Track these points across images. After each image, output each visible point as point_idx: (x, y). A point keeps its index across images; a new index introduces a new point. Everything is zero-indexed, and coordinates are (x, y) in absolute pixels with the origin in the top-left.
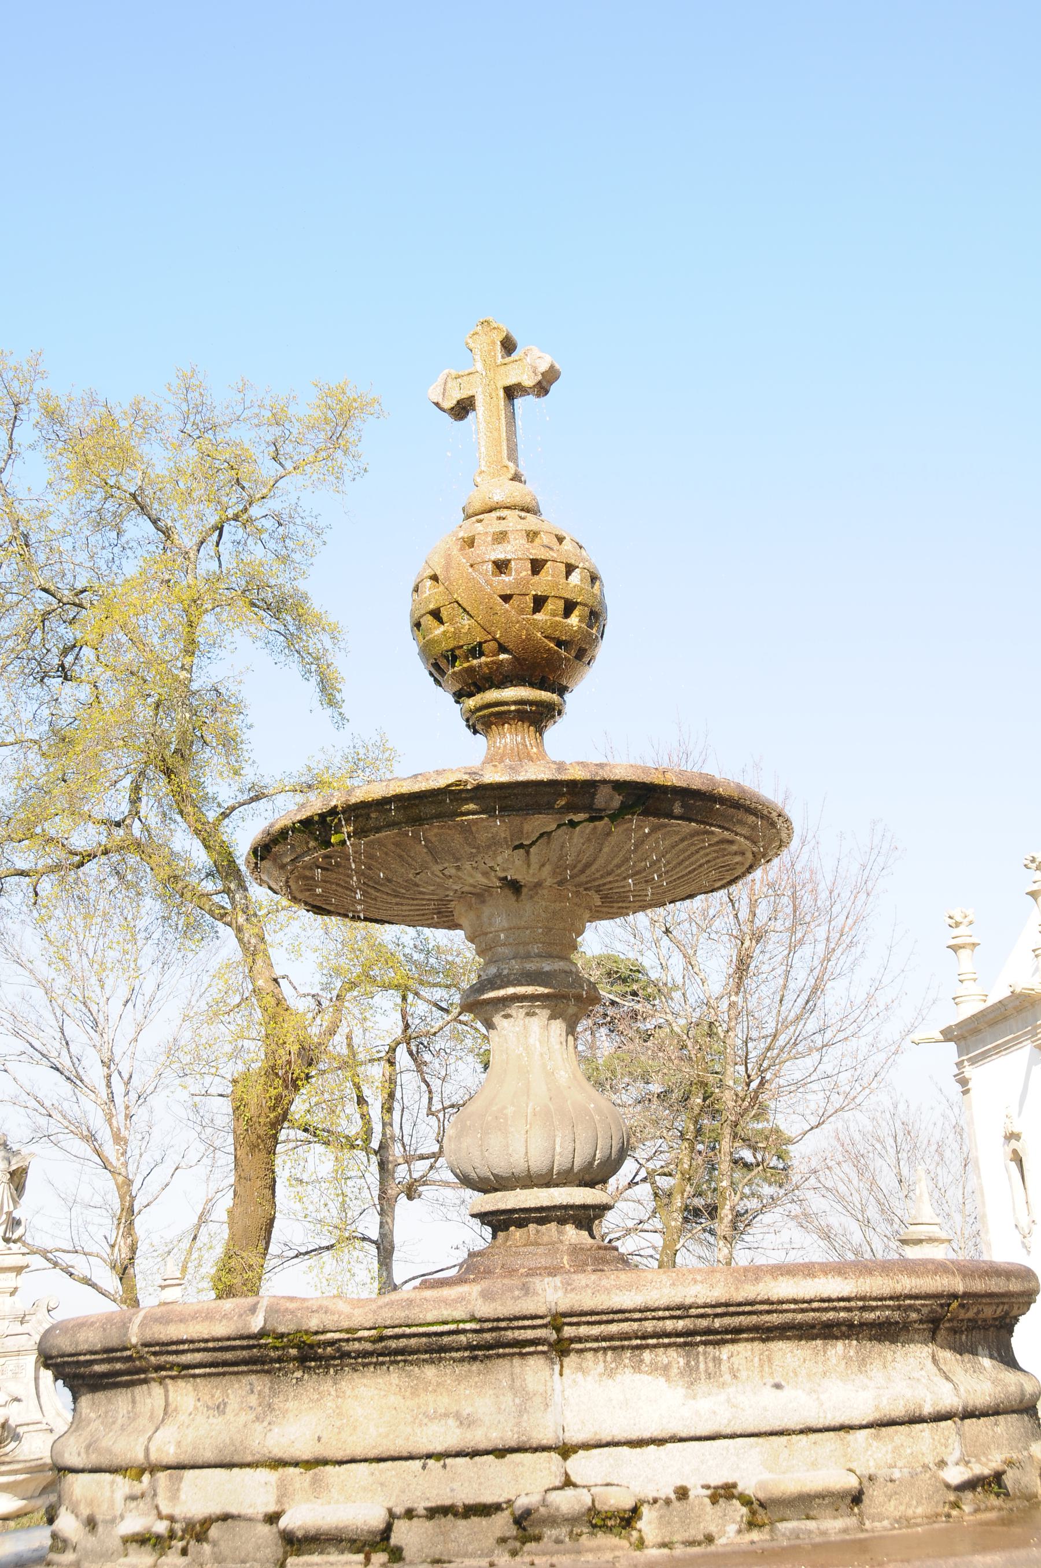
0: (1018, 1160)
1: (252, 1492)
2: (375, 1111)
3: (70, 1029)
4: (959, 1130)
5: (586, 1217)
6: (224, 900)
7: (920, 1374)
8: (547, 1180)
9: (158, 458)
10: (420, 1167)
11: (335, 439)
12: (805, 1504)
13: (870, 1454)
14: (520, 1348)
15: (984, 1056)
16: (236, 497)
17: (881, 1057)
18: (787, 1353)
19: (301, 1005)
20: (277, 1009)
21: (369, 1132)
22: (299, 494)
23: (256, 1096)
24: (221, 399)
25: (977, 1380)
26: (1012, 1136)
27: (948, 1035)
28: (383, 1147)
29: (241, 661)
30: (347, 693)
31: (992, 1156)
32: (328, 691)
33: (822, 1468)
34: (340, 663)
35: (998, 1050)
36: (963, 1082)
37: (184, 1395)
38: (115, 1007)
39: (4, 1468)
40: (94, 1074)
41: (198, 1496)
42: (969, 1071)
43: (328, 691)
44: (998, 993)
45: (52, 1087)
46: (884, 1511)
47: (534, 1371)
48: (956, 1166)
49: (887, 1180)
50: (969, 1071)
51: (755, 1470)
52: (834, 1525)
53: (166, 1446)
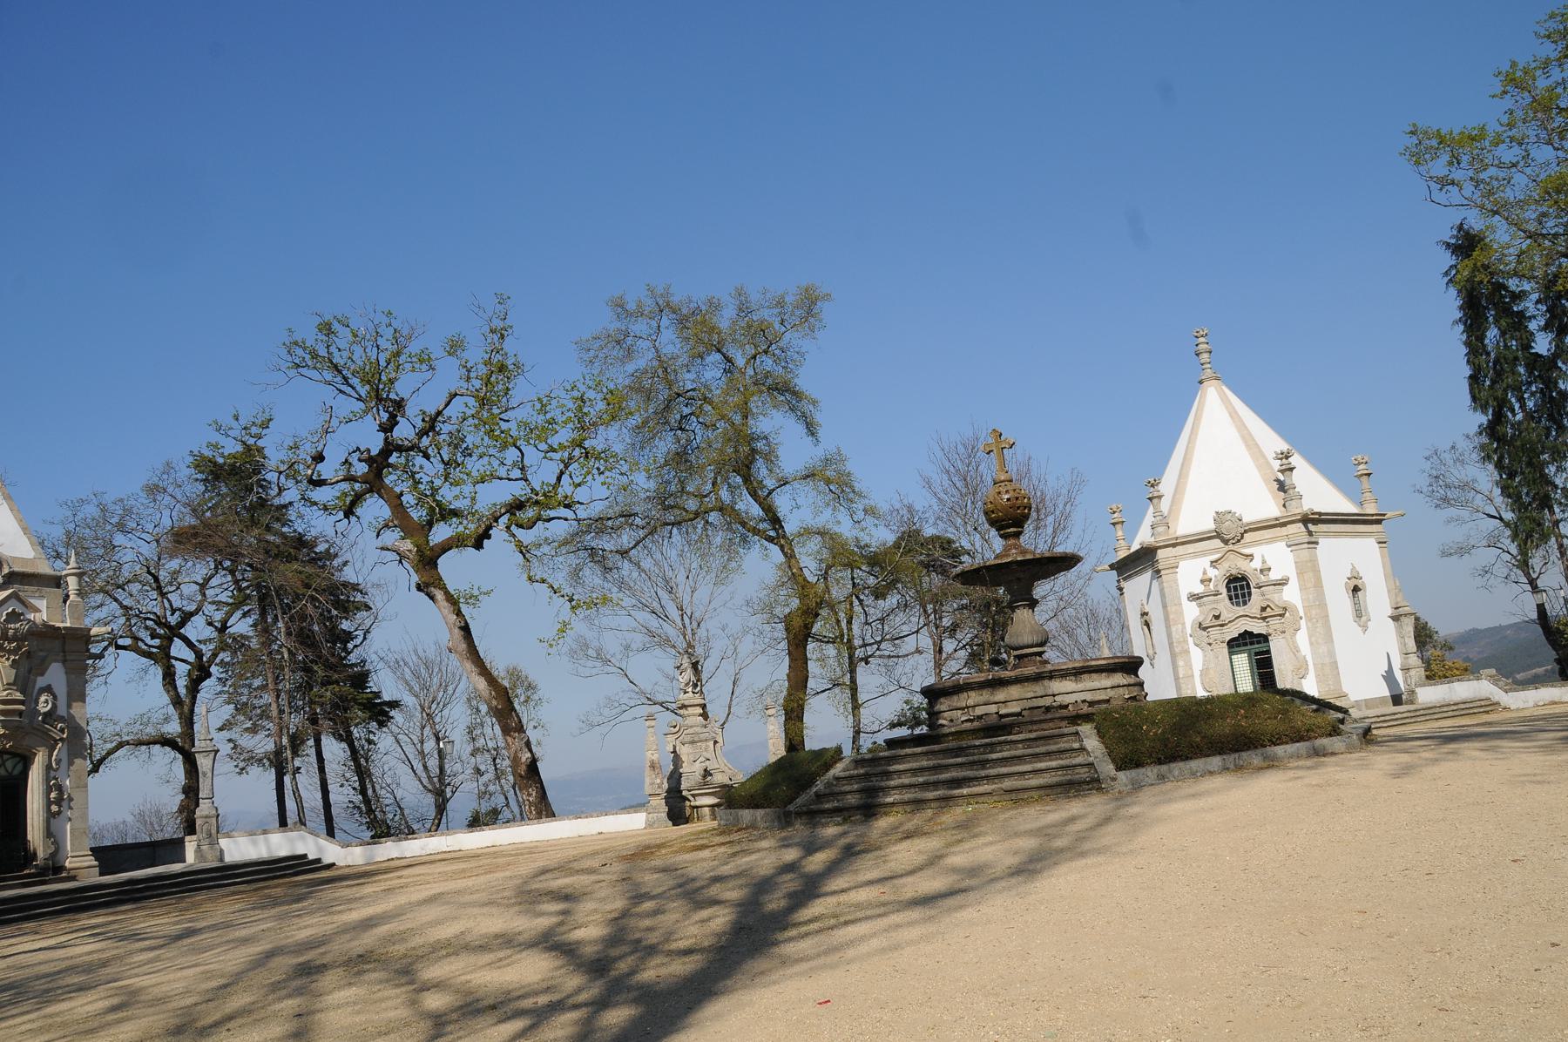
0: (1147, 624)
1: (993, 709)
2: (844, 624)
3: (660, 593)
4: (1119, 611)
5: (1040, 654)
6: (772, 533)
7: (1119, 679)
8: (1032, 646)
9: (725, 320)
10: (870, 650)
11: (809, 312)
12: (1099, 702)
13: (1111, 693)
14: (1043, 678)
15: (1130, 577)
16: (762, 338)
17: (1081, 582)
18: (1094, 676)
19: (812, 579)
20: (805, 584)
21: (842, 635)
22: (791, 338)
23: (797, 622)
24: (754, 297)
25: (1132, 679)
26: (1144, 614)
27: (1112, 567)
28: (849, 640)
29: (773, 422)
30: (821, 433)
31: (1134, 622)
32: (811, 428)
33: (1102, 696)
34: (818, 417)
35: (1137, 574)
36: (1121, 589)
37: (972, 694)
38: (681, 578)
39: (4, 1024)
40: (674, 614)
41: (979, 711)
42: (1123, 584)
43: (811, 428)
44: (1135, 547)
45: (653, 622)
46: (1114, 703)
47: (1046, 682)
48: (1118, 629)
49: (1083, 639)
50: (1123, 584)
51: (1089, 697)
52: (1105, 706)
53: (970, 702)
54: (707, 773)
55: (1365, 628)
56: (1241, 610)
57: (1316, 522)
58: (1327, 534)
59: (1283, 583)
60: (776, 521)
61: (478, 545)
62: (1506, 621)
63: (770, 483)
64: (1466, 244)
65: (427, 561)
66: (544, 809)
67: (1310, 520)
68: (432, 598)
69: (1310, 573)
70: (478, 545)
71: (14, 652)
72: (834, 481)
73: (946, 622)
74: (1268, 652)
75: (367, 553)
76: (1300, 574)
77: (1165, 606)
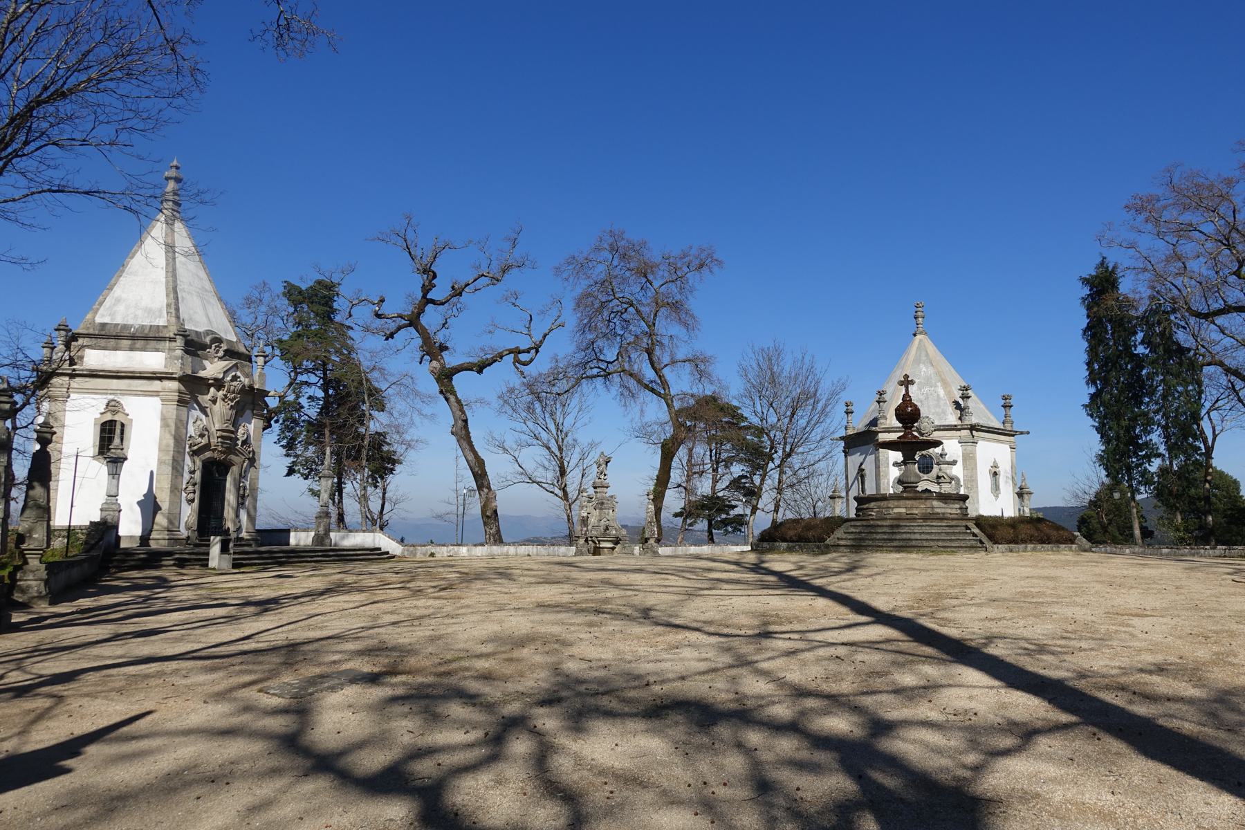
22: (693, 278)
40: (552, 427)
54: (607, 528)
55: (997, 497)
56: (925, 477)
57: (978, 430)
58: (984, 439)
59: (954, 463)
60: (664, 384)
61: (480, 371)
62: (1061, 504)
63: (666, 360)
64: (1102, 285)
65: (445, 378)
66: (498, 540)
67: (973, 428)
68: (447, 399)
69: (969, 459)
70: (480, 371)
71: (232, 400)
72: (698, 364)
73: (724, 456)
74: (208, 554)
75: (393, 363)
76: (965, 460)
77: (846, 470)
